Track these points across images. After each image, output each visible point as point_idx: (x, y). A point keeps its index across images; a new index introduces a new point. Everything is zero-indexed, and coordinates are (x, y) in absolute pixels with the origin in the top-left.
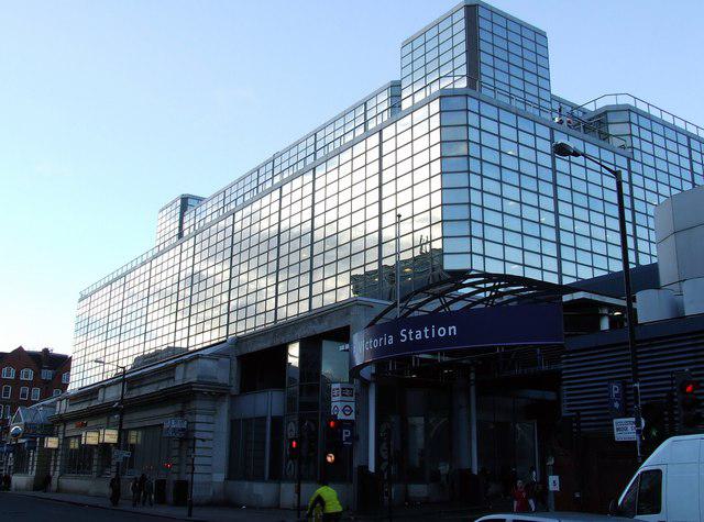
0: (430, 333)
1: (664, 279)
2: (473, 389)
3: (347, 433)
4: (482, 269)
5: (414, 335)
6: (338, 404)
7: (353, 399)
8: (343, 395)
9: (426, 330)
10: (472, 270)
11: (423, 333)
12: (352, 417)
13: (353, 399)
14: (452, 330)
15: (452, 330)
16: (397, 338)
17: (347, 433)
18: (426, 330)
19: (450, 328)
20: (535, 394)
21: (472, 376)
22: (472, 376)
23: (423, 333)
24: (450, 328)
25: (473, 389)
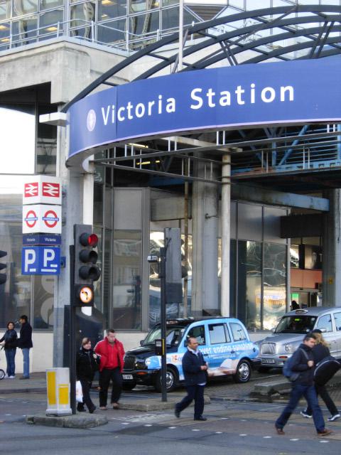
0: (246, 96)
1: (284, 371)
2: (226, 191)
3: (30, 257)
4: (242, 7)
5: (216, 99)
6: (37, 209)
7: (59, 200)
8: (45, 194)
9: (239, 91)
10: (228, 5)
11: (234, 97)
12: (57, 230)
13: (59, 200)
14: (287, 93)
15: (287, 93)
16: (184, 102)
17: (49, 255)
18: (239, 91)
19: (283, 90)
20: (302, 201)
21: (227, 171)
22: (227, 171)
23: (234, 97)
24: (228, 103)
25: (226, 191)
